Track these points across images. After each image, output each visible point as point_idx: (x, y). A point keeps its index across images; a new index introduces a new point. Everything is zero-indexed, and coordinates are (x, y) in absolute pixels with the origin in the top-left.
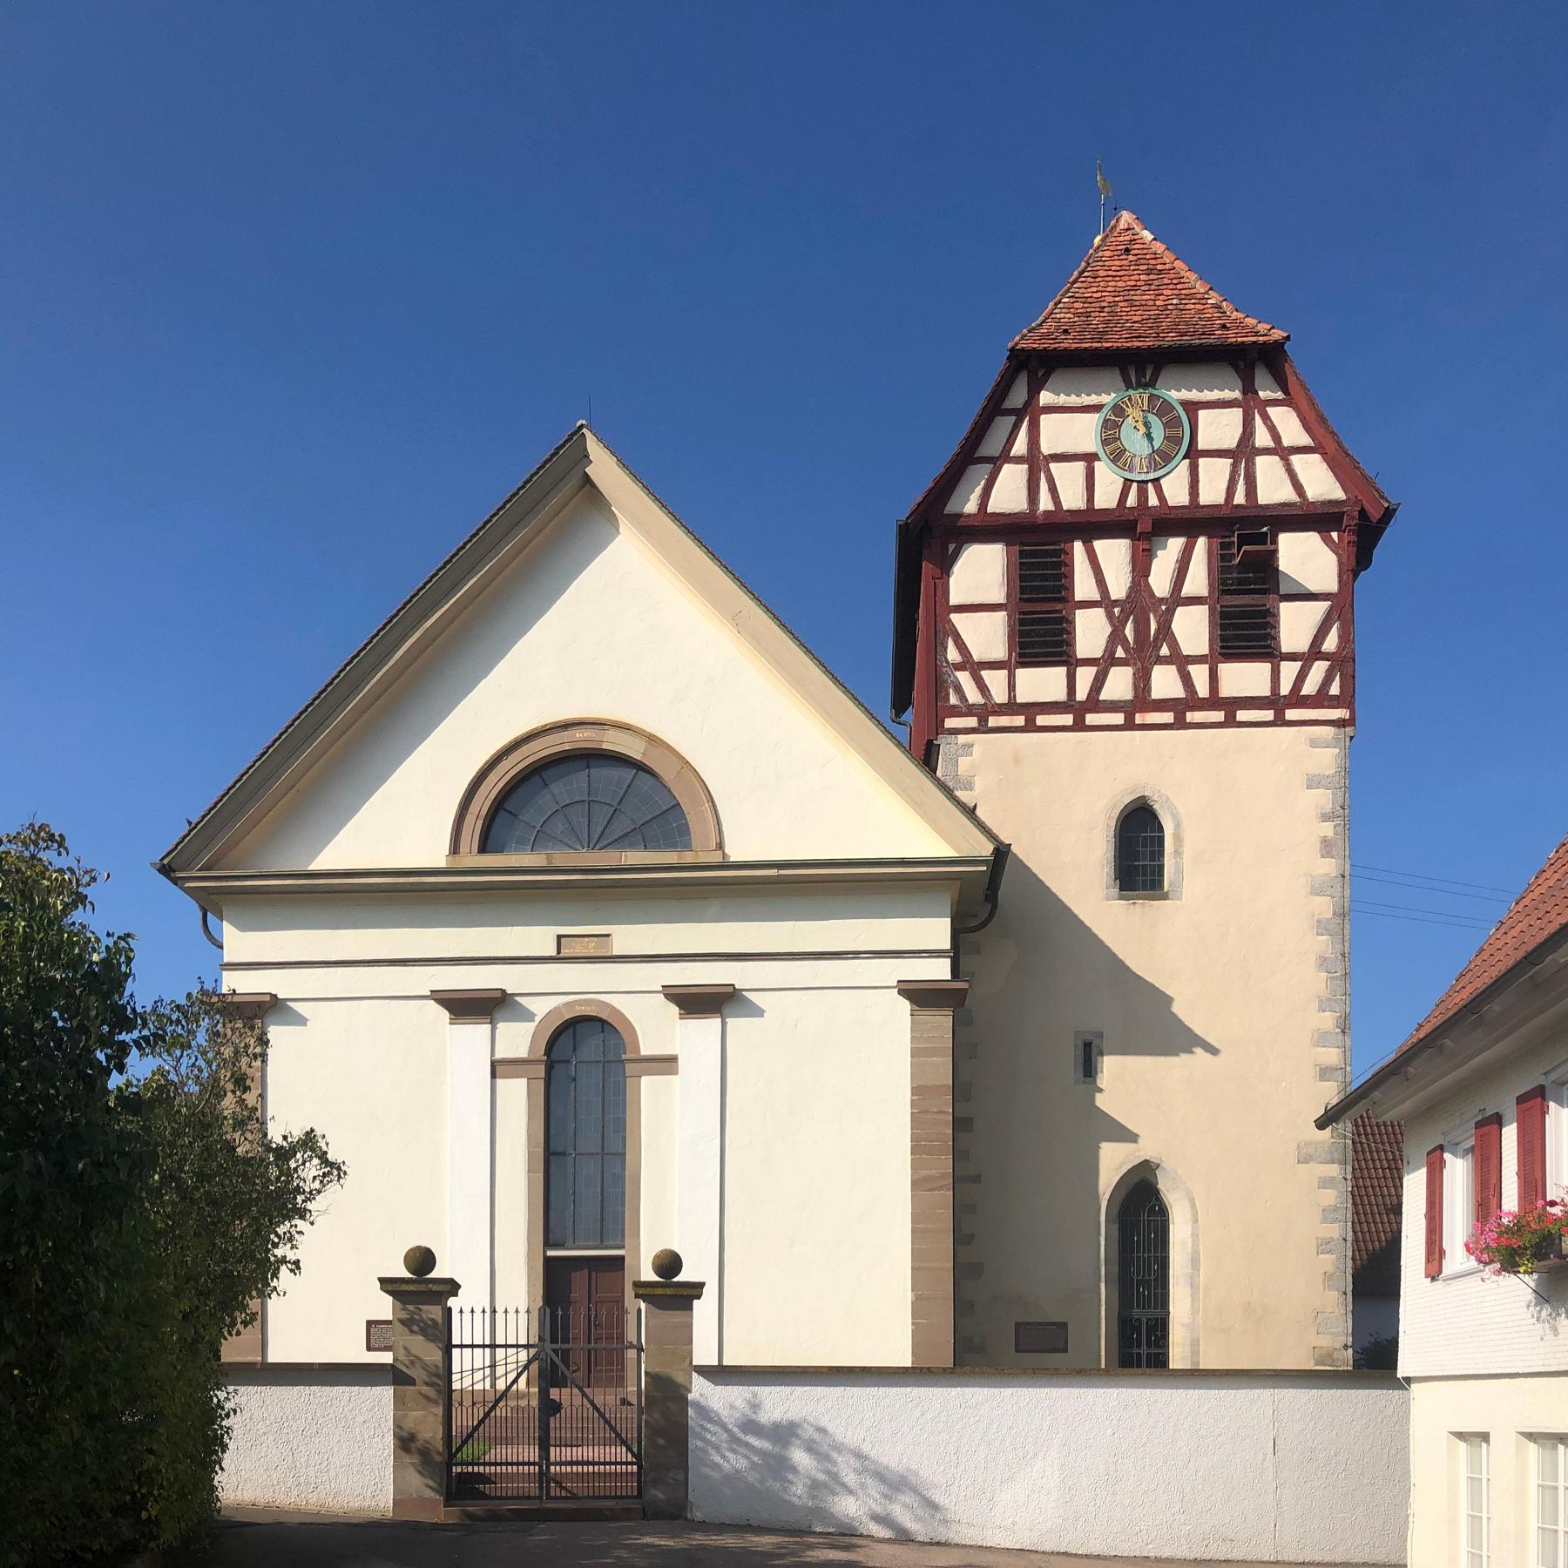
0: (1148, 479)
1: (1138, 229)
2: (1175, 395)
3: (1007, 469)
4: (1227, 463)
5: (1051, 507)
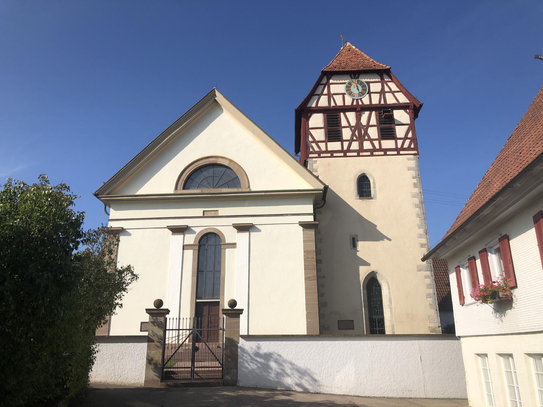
1: (351, 46)
5: (334, 105)
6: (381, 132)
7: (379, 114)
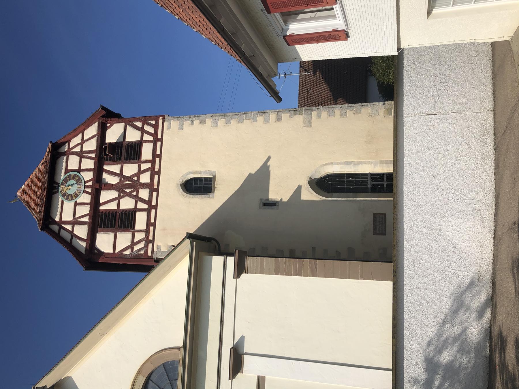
0: (84, 185)
1: (21, 190)
2: (63, 176)
3: (75, 232)
4: (83, 160)
5: (88, 217)
6: (130, 159)
7: (108, 161)
